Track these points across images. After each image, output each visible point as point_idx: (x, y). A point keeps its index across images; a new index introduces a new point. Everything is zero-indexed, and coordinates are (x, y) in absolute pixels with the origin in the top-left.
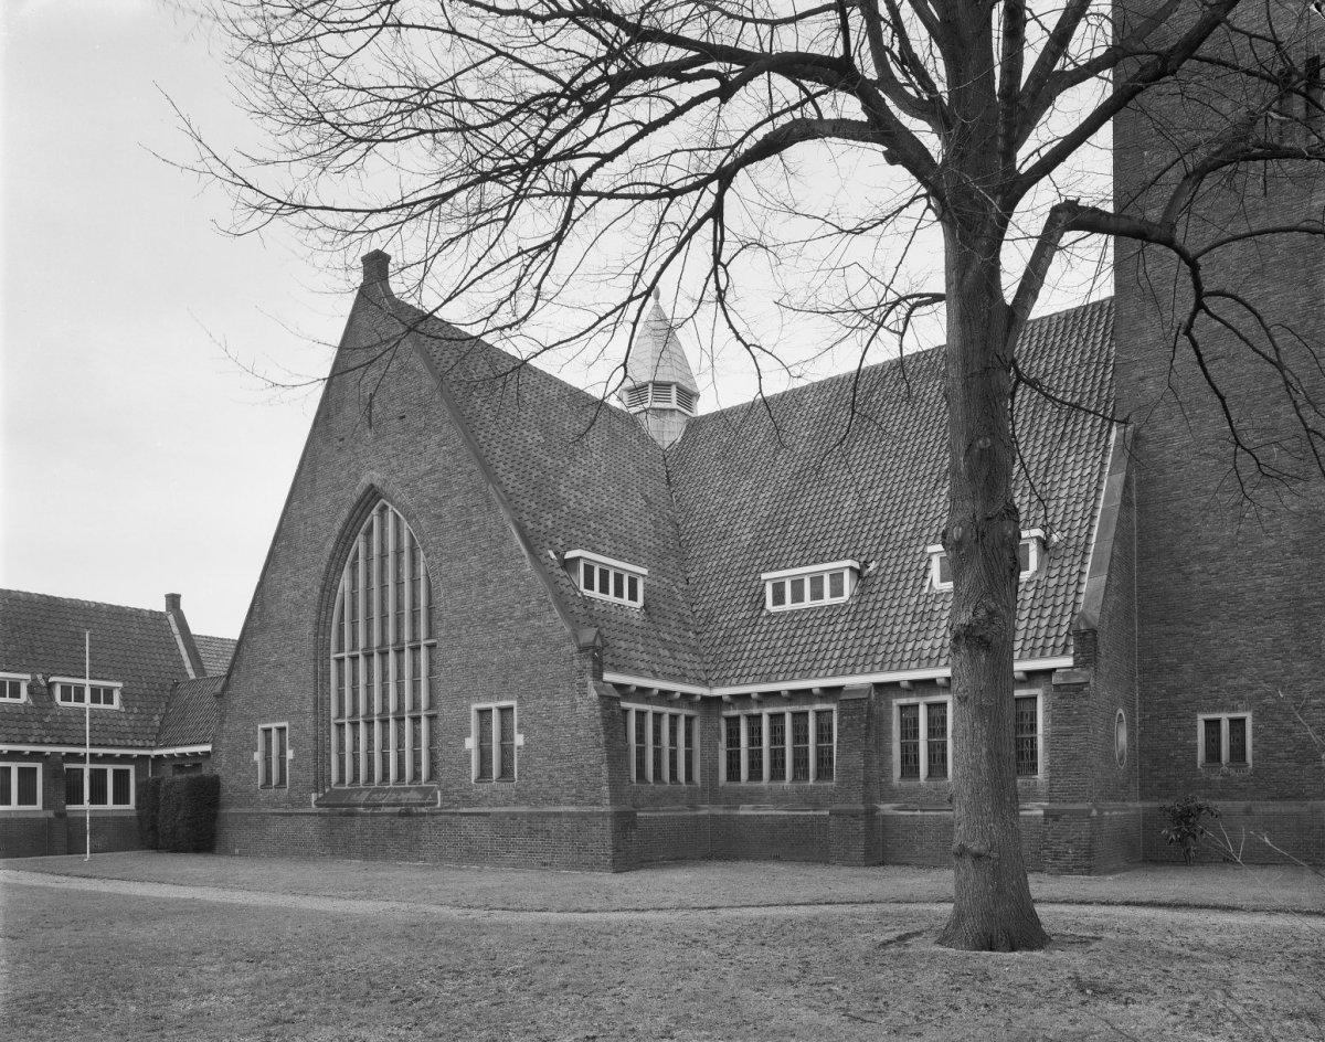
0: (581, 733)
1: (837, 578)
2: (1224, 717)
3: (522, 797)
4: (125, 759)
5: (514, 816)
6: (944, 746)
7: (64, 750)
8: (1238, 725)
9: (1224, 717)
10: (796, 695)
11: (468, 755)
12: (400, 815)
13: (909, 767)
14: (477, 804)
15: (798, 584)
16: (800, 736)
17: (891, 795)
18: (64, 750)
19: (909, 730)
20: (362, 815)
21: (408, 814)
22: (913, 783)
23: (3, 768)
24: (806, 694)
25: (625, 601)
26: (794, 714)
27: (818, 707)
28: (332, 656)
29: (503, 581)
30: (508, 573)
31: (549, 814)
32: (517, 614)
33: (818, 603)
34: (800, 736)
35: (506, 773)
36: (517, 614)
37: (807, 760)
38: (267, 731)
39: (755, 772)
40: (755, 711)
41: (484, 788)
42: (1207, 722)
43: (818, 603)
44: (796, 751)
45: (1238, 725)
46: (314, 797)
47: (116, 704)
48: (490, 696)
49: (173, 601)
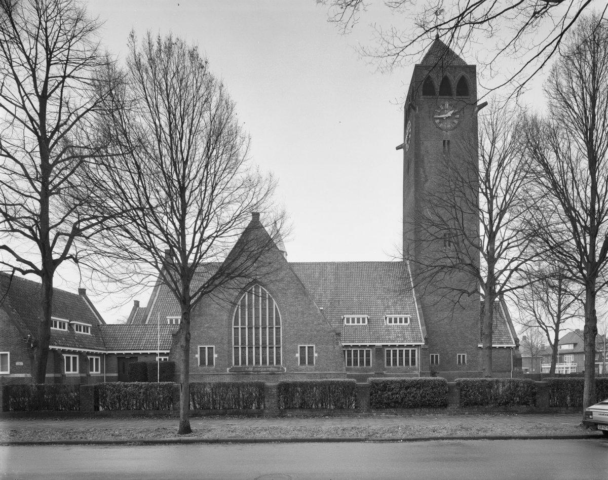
0: (337, 354)
1: (364, 319)
2: (435, 355)
3: (316, 369)
4: (74, 353)
5: (315, 374)
6: (369, 360)
7: (62, 348)
8: (464, 356)
9: (435, 355)
10: (362, 346)
11: (297, 358)
12: (270, 374)
13: (389, 364)
14: (301, 371)
15: (358, 319)
16: (362, 356)
17: (385, 369)
18: (62, 348)
19: (388, 355)
20: (252, 374)
21: (274, 374)
22: (390, 367)
23: (1, 354)
24: (365, 346)
25: (403, 324)
26: (412, 350)
27: (361, 349)
28: (233, 327)
29: (310, 314)
30: (312, 312)
31: (327, 374)
32: (315, 323)
33: (353, 324)
34: (362, 356)
35: (311, 363)
36: (315, 323)
37: (305, 358)
38: (459, 356)
39: (401, 364)
40: (350, 349)
41: (303, 367)
42: (300, 347)
43: (353, 324)
44: (412, 359)
45: (437, 356)
46: (228, 369)
47: (214, 346)
48: (305, 343)
49: (82, 291)
